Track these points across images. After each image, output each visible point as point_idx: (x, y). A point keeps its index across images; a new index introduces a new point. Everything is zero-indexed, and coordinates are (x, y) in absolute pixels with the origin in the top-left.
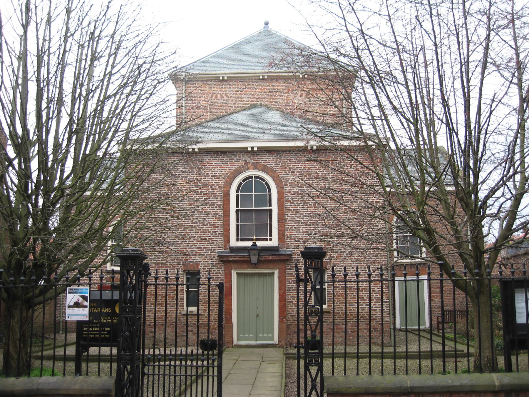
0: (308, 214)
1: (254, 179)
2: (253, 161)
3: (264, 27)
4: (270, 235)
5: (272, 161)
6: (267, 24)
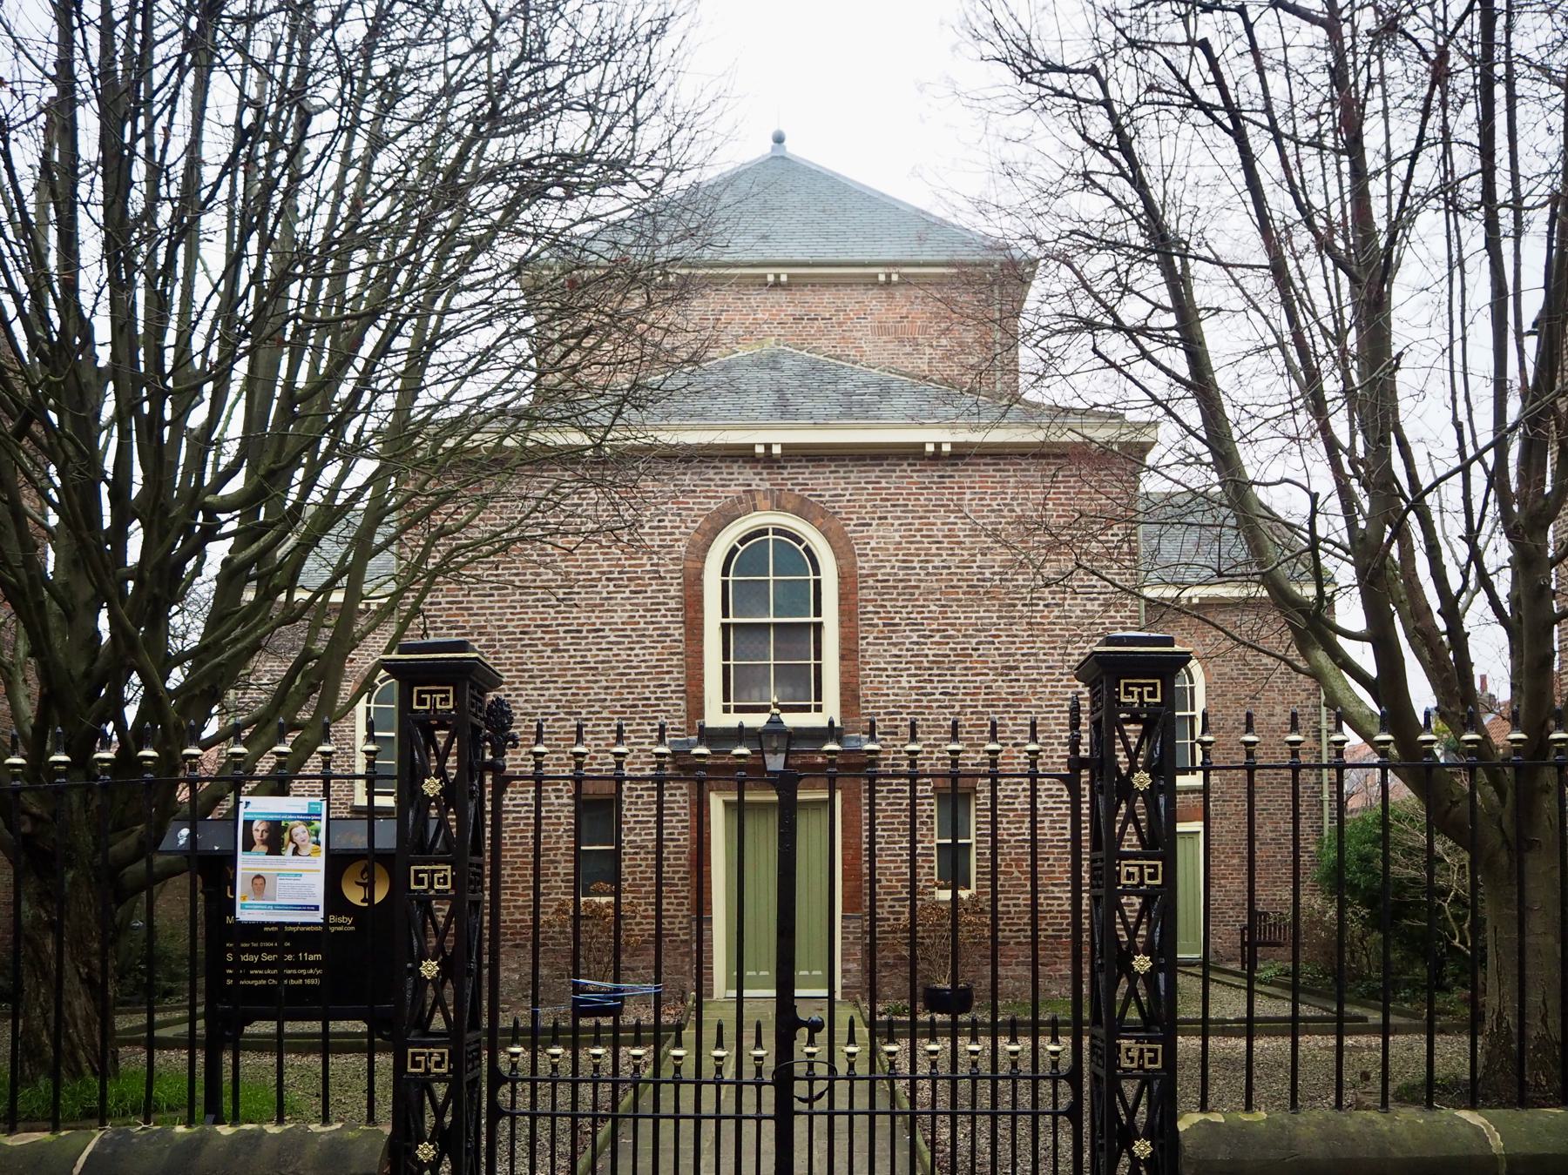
0: (923, 636)
1: (771, 536)
2: (767, 485)
3: (773, 149)
4: (818, 697)
5: (826, 484)
6: (779, 139)
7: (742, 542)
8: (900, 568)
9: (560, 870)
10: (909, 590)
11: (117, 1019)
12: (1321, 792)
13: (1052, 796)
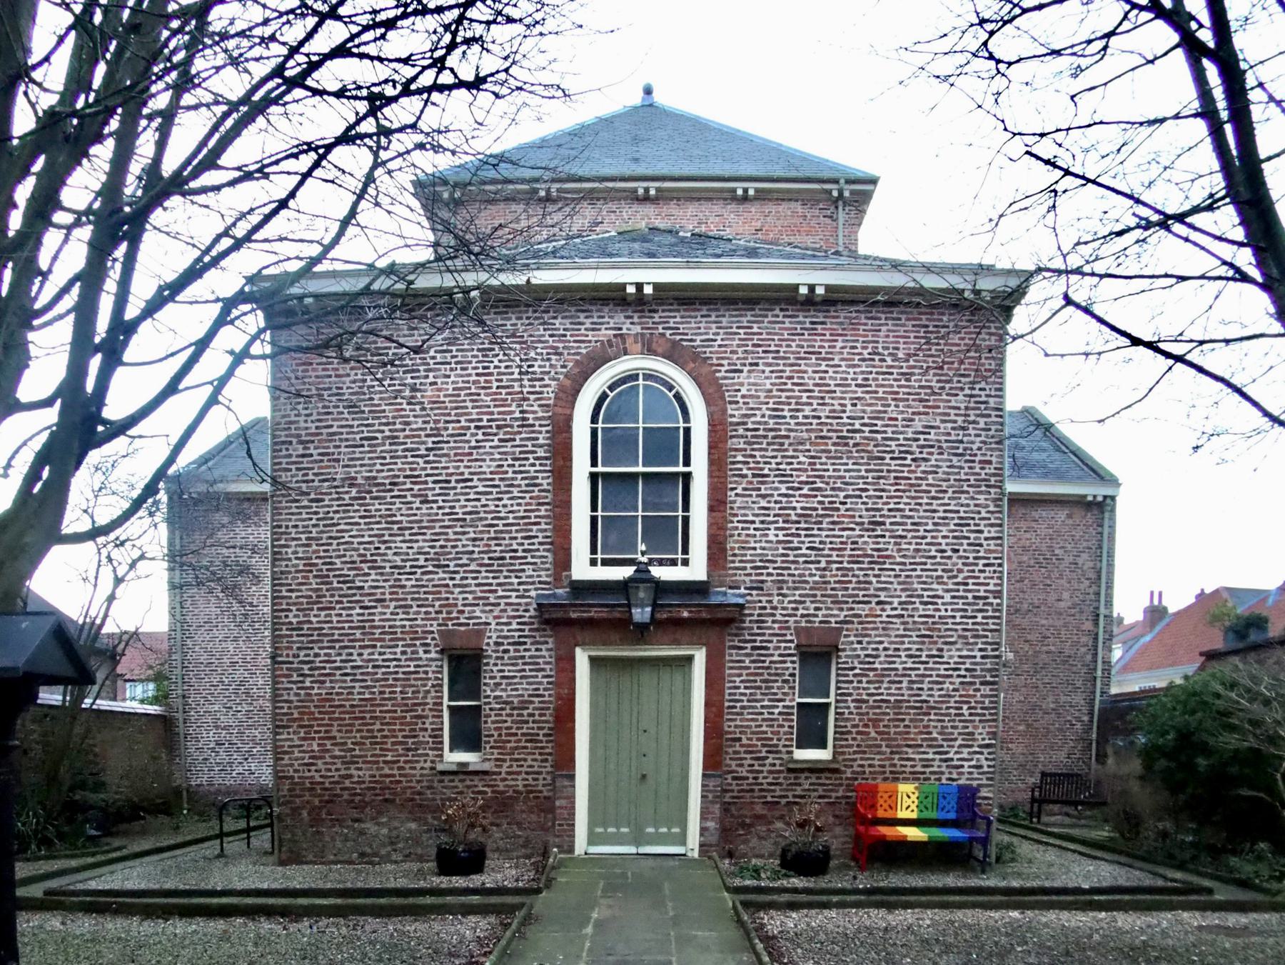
2: (638, 329)
3: (643, 99)
4: (685, 550)
6: (648, 91)
7: (611, 388)
8: (771, 417)
9: (427, 726)
10: (779, 440)
11: (22, 870)
12: (1095, 669)
13: (910, 656)
